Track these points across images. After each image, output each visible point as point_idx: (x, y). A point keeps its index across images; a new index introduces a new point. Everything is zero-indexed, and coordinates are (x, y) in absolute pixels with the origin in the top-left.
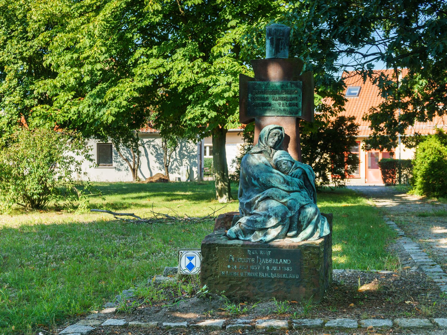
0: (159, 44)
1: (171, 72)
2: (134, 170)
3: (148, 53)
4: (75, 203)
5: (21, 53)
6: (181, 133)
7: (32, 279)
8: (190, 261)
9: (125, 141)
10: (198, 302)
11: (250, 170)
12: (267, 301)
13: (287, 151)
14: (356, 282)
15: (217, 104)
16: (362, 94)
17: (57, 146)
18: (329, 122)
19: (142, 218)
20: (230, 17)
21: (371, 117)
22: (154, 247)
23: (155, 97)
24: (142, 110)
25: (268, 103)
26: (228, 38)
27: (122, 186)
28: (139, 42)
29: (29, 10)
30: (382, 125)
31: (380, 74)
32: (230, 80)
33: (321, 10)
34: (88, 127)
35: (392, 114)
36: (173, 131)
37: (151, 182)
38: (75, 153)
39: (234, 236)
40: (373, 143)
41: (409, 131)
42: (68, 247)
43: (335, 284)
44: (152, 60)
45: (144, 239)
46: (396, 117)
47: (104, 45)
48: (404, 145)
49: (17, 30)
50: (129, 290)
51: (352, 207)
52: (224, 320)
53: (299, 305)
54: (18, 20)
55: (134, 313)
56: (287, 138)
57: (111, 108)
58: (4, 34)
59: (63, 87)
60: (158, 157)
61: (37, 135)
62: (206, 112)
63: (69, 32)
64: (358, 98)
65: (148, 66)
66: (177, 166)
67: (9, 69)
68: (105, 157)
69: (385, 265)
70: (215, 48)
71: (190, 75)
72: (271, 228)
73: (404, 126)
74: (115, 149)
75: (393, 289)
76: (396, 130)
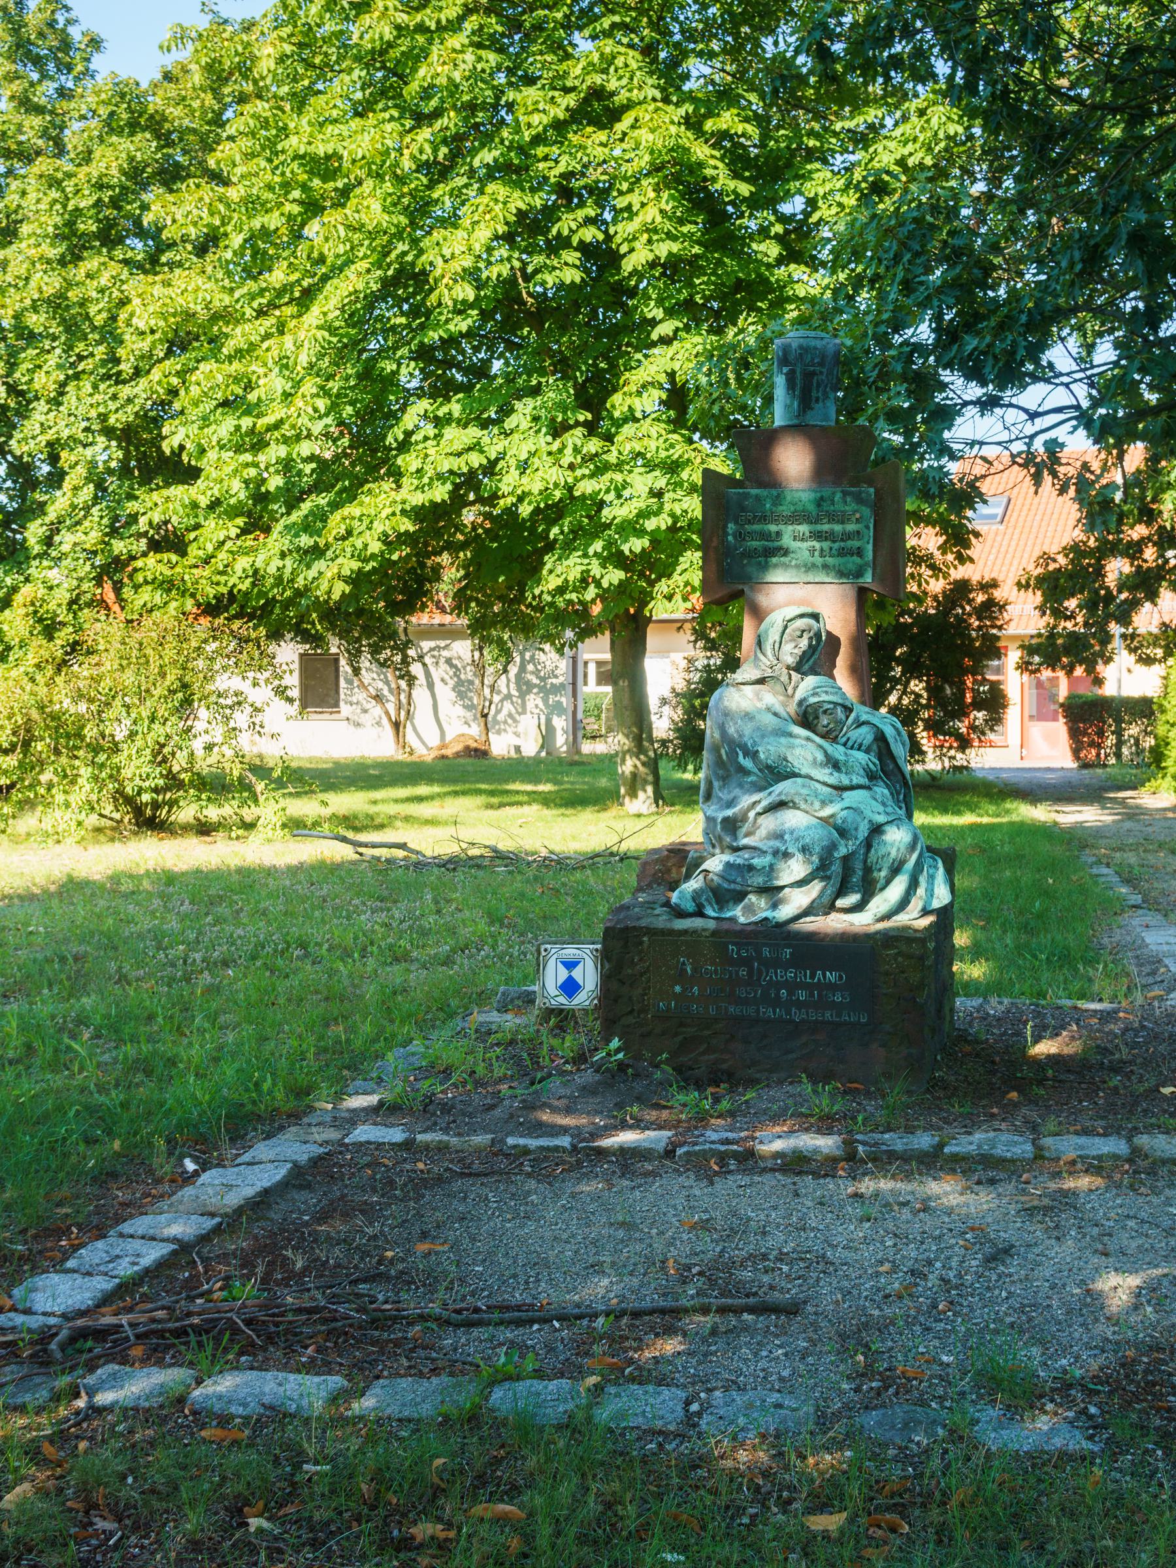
0: (467, 388)
1: (501, 464)
2: (396, 725)
3: (440, 413)
4: (248, 814)
5: (103, 418)
6: (526, 628)
7: (151, 1018)
8: (571, 972)
9: (375, 650)
10: (598, 1083)
11: (731, 730)
12: (780, 1082)
13: (832, 677)
14: (1020, 1034)
15: (625, 548)
16: (1013, 516)
17: (201, 664)
18: (925, 593)
19: (429, 853)
20: (659, 313)
21: (1041, 581)
22: (465, 932)
23: (457, 529)
24: (422, 565)
25: (780, 548)
26: (653, 369)
27: (368, 767)
28: (415, 384)
29: (123, 302)
30: (1072, 604)
31: (1078, 464)
32: (661, 483)
33: (914, 290)
34: (277, 611)
35: (1100, 573)
36: (504, 621)
37: (443, 757)
38: (249, 682)
39: (690, 907)
40: (1048, 651)
41: (1146, 619)
42: (240, 932)
43: (963, 1037)
44: (450, 432)
45: (439, 912)
46: (1111, 580)
47: (324, 392)
48: (1133, 658)
49: (92, 355)
50: (411, 1048)
51: (991, 828)
52: (669, 1134)
53: (868, 1094)
54: (94, 328)
55: (428, 1110)
56: (833, 642)
57: (340, 560)
58: (59, 367)
59: (214, 505)
60: (462, 689)
61: (148, 631)
62: (596, 570)
63: (230, 359)
64: (1002, 527)
65: (436, 448)
66: (510, 715)
67: (73, 458)
68: (319, 690)
69: (1096, 988)
70: (617, 398)
71: (555, 475)
72: (792, 885)
73: (1134, 604)
74: (349, 669)
75: (1125, 1053)
76: (1109, 617)
